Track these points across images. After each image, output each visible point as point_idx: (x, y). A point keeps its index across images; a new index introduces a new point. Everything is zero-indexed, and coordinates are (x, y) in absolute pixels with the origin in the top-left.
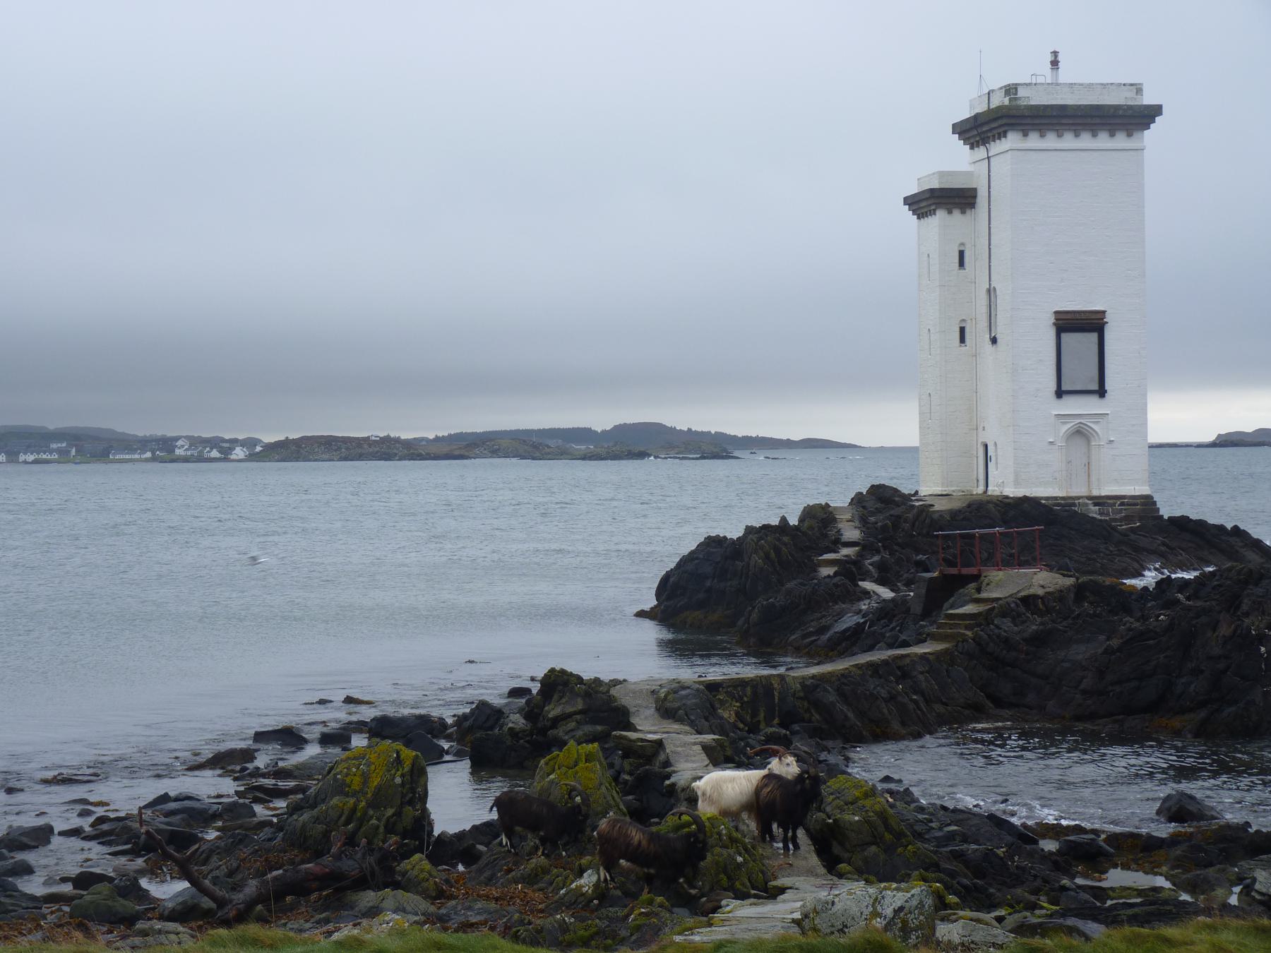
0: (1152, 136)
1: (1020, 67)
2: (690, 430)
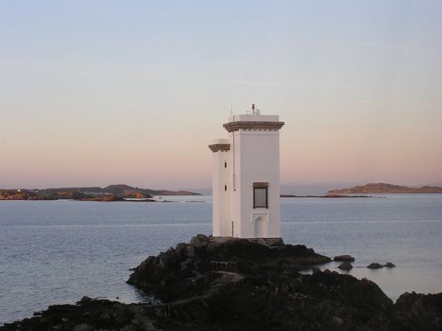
0: (282, 130)
1: (241, 111)
2: (414, 292)
